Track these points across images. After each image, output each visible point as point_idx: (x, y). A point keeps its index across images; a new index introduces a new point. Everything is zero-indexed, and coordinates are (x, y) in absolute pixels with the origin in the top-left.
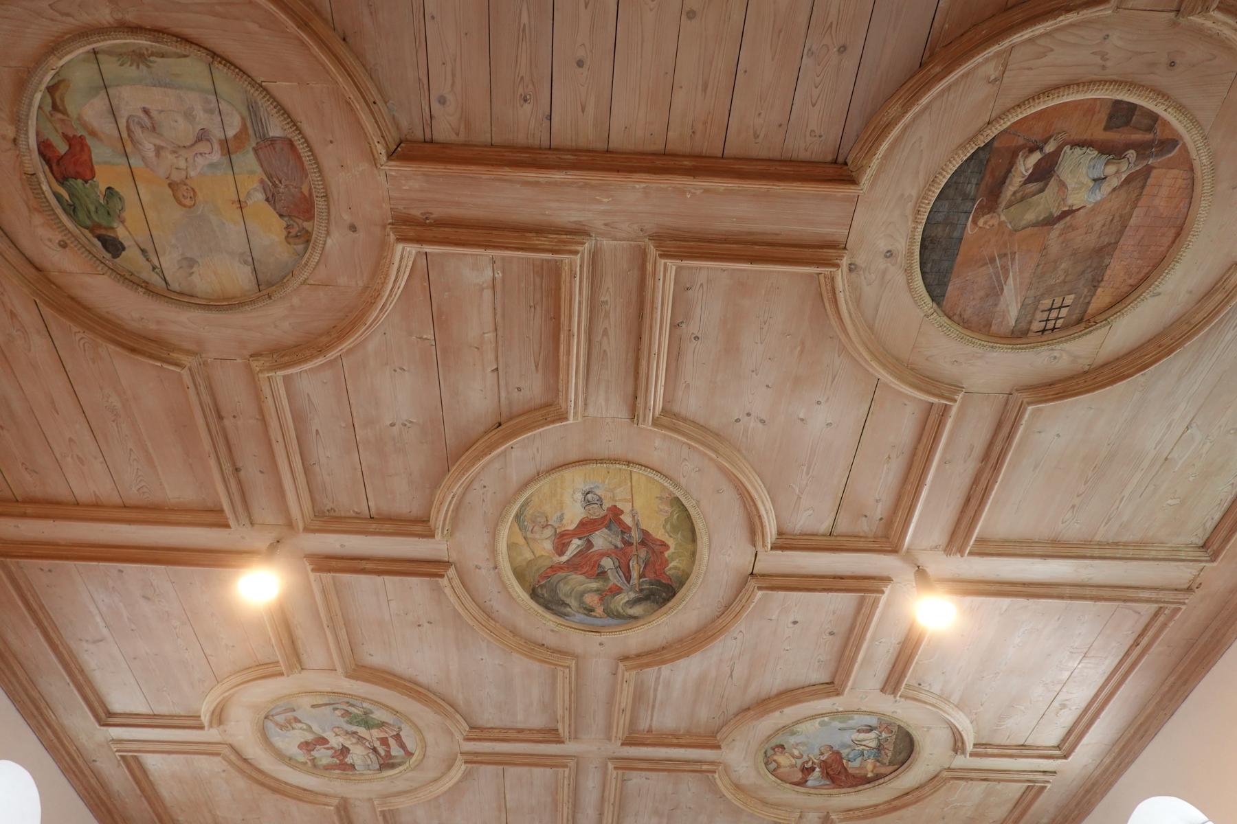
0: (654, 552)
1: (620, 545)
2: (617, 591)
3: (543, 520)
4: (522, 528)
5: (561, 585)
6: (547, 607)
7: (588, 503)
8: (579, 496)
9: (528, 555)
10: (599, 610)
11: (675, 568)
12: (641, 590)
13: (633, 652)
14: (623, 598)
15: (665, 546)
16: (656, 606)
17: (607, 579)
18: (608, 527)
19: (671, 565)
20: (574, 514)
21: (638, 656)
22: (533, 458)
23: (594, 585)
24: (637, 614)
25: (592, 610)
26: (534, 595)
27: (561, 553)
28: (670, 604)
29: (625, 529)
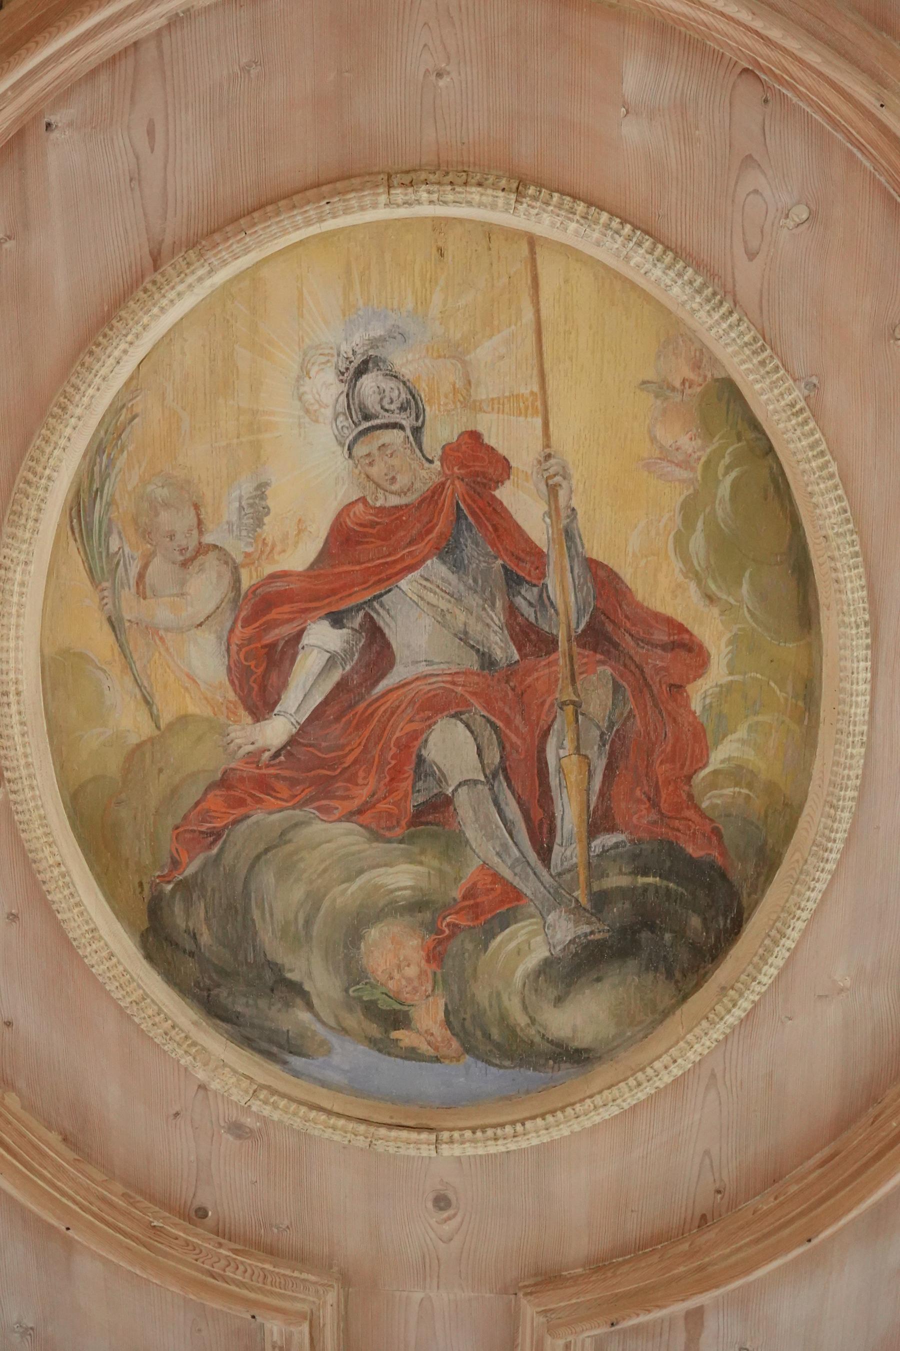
0: (643, 685)
1: (502, 648)
2: (493, 907)
3: (178, 521)
4: (102, 571)
5: (267, 877)
6: (214, 1010)
7: (363, 422)
8: (326, 387)
9: (129, 721)
10: (429, 1018)
11: (737, 773)
12: (601, 901)
13: (578, 1247)
14: (530, 943)
15: (685, 647)
16: (664, 993)
17: (453, 844)
18: (448, 551)
19: (720, 755)
20: (307, 485)
21: (600, 1265)
22: (136, 178)
23: (402, 876)
24: (585, 1039)
25: (397, 1019)
26: (159, 940)
27: (260, 700)
28: (723, 973)
29: (520, 565)
